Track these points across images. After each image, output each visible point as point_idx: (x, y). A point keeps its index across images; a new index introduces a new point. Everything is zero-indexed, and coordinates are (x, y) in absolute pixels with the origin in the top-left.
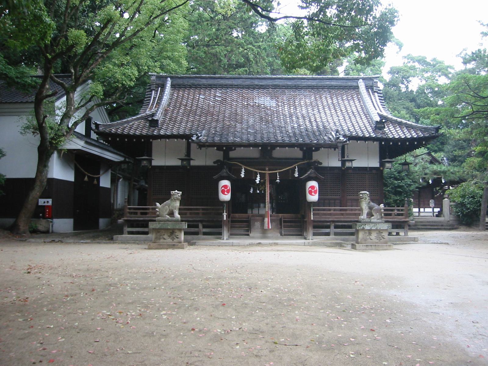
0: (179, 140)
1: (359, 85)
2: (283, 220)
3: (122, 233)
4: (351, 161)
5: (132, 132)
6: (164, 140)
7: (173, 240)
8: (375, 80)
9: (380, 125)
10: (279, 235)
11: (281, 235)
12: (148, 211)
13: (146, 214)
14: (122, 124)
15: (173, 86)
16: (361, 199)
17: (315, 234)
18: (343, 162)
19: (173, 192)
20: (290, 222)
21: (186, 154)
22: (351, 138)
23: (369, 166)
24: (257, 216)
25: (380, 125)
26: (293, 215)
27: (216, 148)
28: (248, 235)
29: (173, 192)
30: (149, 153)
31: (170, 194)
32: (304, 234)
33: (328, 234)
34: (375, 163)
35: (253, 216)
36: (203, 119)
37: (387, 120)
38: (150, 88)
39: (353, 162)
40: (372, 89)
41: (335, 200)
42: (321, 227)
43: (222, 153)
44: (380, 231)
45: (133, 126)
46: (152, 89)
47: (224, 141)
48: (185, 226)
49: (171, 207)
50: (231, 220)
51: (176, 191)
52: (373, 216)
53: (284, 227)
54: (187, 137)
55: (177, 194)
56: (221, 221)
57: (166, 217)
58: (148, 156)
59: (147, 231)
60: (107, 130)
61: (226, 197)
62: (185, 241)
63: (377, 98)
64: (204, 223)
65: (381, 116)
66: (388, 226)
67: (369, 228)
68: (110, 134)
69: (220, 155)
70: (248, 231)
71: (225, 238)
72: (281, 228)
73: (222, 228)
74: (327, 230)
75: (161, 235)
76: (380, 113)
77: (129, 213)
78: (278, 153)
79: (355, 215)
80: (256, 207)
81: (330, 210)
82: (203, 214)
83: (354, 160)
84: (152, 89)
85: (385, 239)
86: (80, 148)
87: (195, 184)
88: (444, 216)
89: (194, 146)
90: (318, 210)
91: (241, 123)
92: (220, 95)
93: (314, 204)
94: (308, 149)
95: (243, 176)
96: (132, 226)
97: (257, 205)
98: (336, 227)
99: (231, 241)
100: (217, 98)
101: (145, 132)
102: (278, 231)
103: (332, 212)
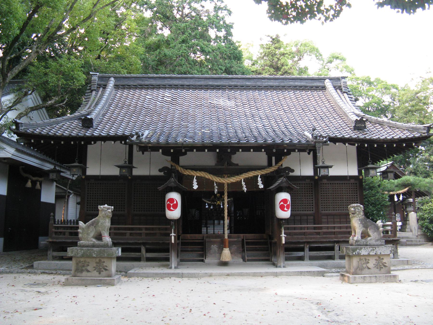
2: (245, 241)
4: (328, 167)
7: (100, 273)
9: (360, 125)
11: (244, 260)
15: (117, 87)
17: (287, 259)
18: (315, 170)
19: (102, 206)
20: (253, 243)
24: (213, 237)
26: (257, 235)
28: (203, 261)
29: (101, 207)
30: (83, 160)
31: (98, 210)
32: (273, 260)
34: (353, 171)
35: (208, 237)
38: (90, 89)
40: (341, 90)
41: (307, 215)
42: (294, 251)
43: (169, 158)
45: (67, 126)
46: (92, 89)
47: (171, 141)
48: (119, 252)
50: (182, 243)
51: (106, 205)
52: (369, 236)
53: (247, 250)
56: (169, 244)
57: (92, 241)
60: (30, 131)
61: (175, 214)
62: (119, 271)
64: (147, 246)
67: (366, 253)
69: (166, 161)
70: (202, 256)
71: (173, 266)
72: (243, 251)
73: (168, 252)
74: (301, 254)
75: (83, 266)
77: (56, 233)
78: (239, 158)
79: (334, 234)
80: (210, 224)
82: (147, 234)
83: (331, 167)
86: (9, 156)
88: (411, 231)
93: (287, 221)
94: (277, 151)
97: (212, 222)
98: (311, 249)
99: (178, 271)
101: (74, 133)
102: (240, 255)
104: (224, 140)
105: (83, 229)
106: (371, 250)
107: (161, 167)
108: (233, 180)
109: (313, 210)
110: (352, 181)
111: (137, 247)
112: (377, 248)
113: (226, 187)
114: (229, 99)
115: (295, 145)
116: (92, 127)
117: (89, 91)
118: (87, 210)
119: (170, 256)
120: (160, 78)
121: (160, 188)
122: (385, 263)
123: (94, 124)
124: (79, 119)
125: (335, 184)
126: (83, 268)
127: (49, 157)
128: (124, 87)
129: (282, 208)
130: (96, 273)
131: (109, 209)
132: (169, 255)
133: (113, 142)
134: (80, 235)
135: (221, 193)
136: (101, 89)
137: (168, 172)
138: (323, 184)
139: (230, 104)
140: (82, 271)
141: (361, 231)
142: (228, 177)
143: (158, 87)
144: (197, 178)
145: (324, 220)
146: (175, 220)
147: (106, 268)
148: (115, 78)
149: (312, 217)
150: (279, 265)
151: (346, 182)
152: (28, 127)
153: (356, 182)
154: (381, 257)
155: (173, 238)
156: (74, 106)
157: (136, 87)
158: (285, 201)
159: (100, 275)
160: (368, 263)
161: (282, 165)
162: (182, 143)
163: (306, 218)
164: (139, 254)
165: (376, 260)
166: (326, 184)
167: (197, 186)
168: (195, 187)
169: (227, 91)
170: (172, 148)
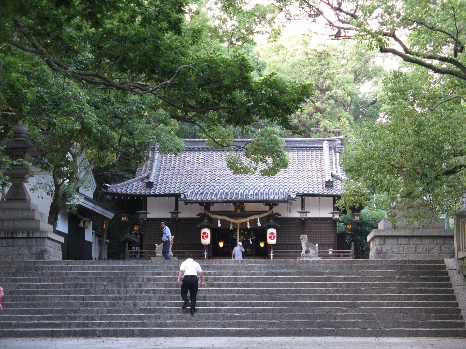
5: (133, 192)
9: (329, 185)
12: (143, 254)
14: (125, 185)
23: (321, 217)
36: (188, 181)
43: (203, 208)
45: (132, 187)
47: (204, 198)
52: (310, 252)
54: (177, 196)
69: (201, 210)
78: (248, 207)
81: (290, 252)
89: (181, 203)
90: (278, 252)
91: (219, 183)
92: (203, 157)
101: (143, 192)
103: (292, 254)
105: (158, 248)
108: (243, 221)
113: (239, 225)
120: (195, 142)
121: (198, 226)
129: (270, 238)
135: (235, 230)
137: (202, 217)
142: (240, 219)
144: (220, 220)
155: (206, 256)
158: (272, 234)
161: (273, 212)
168: (219, 225)
170: (205, 203)
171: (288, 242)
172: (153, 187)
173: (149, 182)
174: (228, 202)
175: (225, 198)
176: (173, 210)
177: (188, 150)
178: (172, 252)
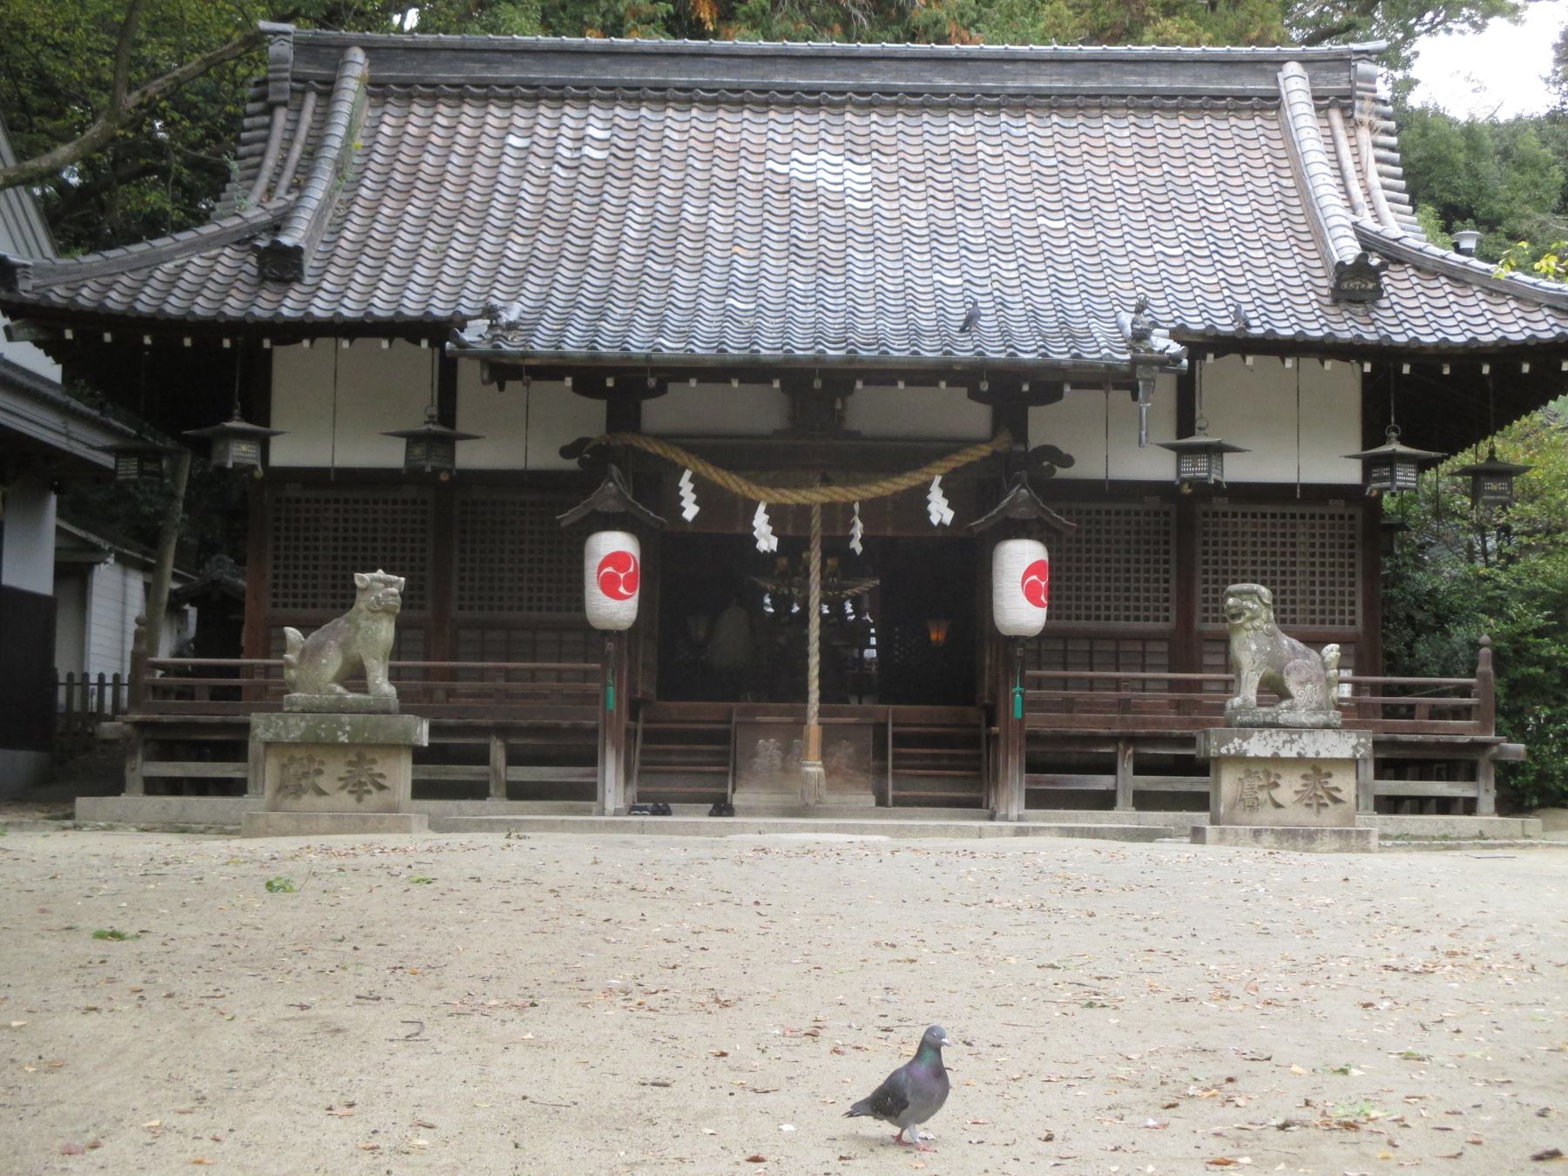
0: (400, 342)
1: (1283, 93)
3: (115, 787)
5: (174, 306)
6: (330, 341)
7: (359, 800)
8: (1363, 67)
9: (1356, 284)
10: (871, 800)
13: (234, 693)
15: (378, 90)
16: (1233, 617)
17: (1036, 800)
19: (367, 576)
21: (434, 411)
22: (1205, 345)
25: (1355, 284)
27: (568, 381)
29: (362, 579)
33: (1105, 801)
36: (516, 249)
37: (1395, 256)
39: (1226, 455)
41: (1145, 638)
43: (599, 407)
44: (1317, 768)
45: (188, 275)
46: (272, 98)
47: (606, 347)
49: (351, 652)
50: (645, 732)
51: (380, 573)
55: (380, 586)
57: (332, 692)
58: (248, 421)
59: (238, 775)
60: (59, 294)
63: (1369, 154)
64: (513, 741)
65: (1368, 242)
66: (1354, 741)
67: (1268, 753)
68: (70, 315)
69: (590, 418)
74: (1103, 782)
75: (305, 775)
76: (1368, 223)
78: (870, 412)
84: (272, 98)
85: (1341, 806)
87: (465, 539)
89: (469, 375)
95: (690, 511)
96: (167, 752)
100: (587, 150)
101: (234, 306)
104: (801, 347)
106: (1285, 742)
107: (569, 440)
109: (1167, 619)
110: (1337, 507)
111: (471, 741)
112: (1305, 736)
114: (851, 153)
115: (1057, 368)
116: (299, 281)
117: (258, 106)
118: (275, 605)
119: (599, 780)
121: (567, 518)
122: (1338, 790)
123: (307, 271)
124: (238, 243)
125: (1264, 516)
126: (303, 783)
127: (694, 491)
128: (408, 92)
130: (346, 799)
131: (388, 584)
132: (595, 775)
133: (385, 344)
134: (292, 674)
136: (311, 100)
137: (592, 460)
138: (1215, 514)
139: (857, 176)
140: (298, 792)
141: (1258, 679)
143: (558, 95)
145: (1208, 660)
146: (620, 633)
147: (380, 781)
148: (369, 49)
149: (1164, 647)
150: (1003, 812)
151: (1289, 510)
152: (47, 281)
153: (1350, 511)
154: (1325, 770)
156: (203, 184)
157: (460, 94)
159: (361, 807)
160: (1276, 785)
162: (648, 358)
163: (1140, 648)
164: (484, 768)
165: (1304, 777)
166: (1225, 515)
167: (696, 509)
168: (690, 511)
169: (848, 117)
171: (1092, 625)
172: (298, 279)
173: (278, 251)
174: (753, 371)
175: (735, 347)
176: (419, 414)
177: (524, 98)
178: (395, 675)
